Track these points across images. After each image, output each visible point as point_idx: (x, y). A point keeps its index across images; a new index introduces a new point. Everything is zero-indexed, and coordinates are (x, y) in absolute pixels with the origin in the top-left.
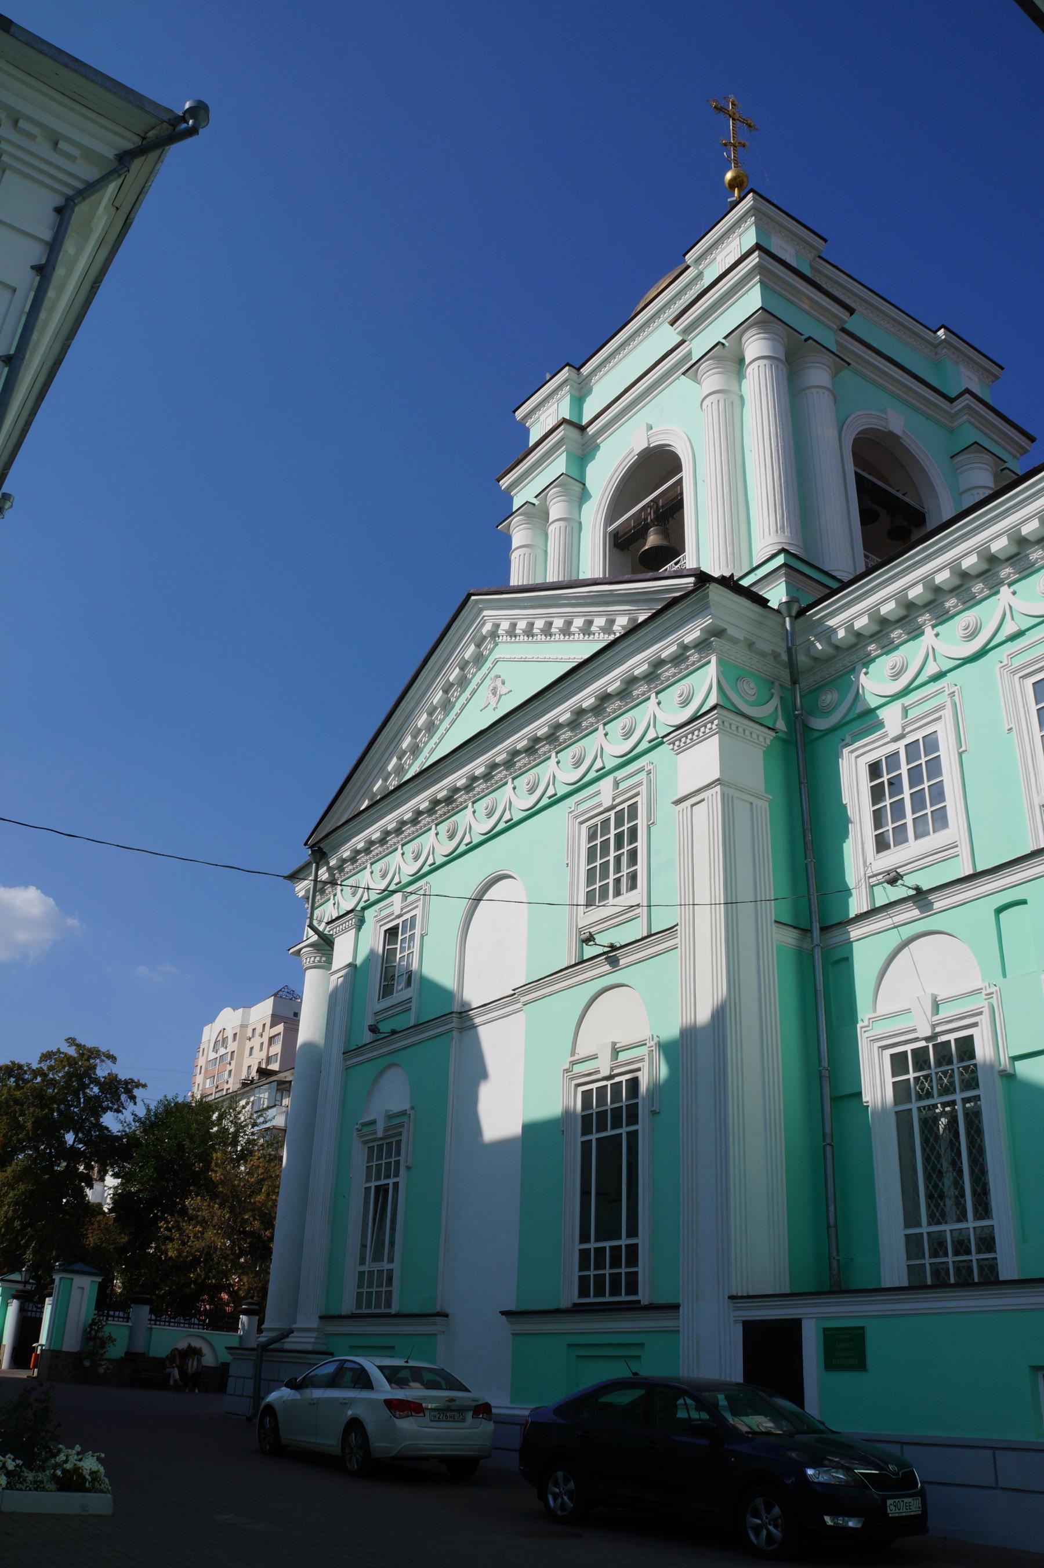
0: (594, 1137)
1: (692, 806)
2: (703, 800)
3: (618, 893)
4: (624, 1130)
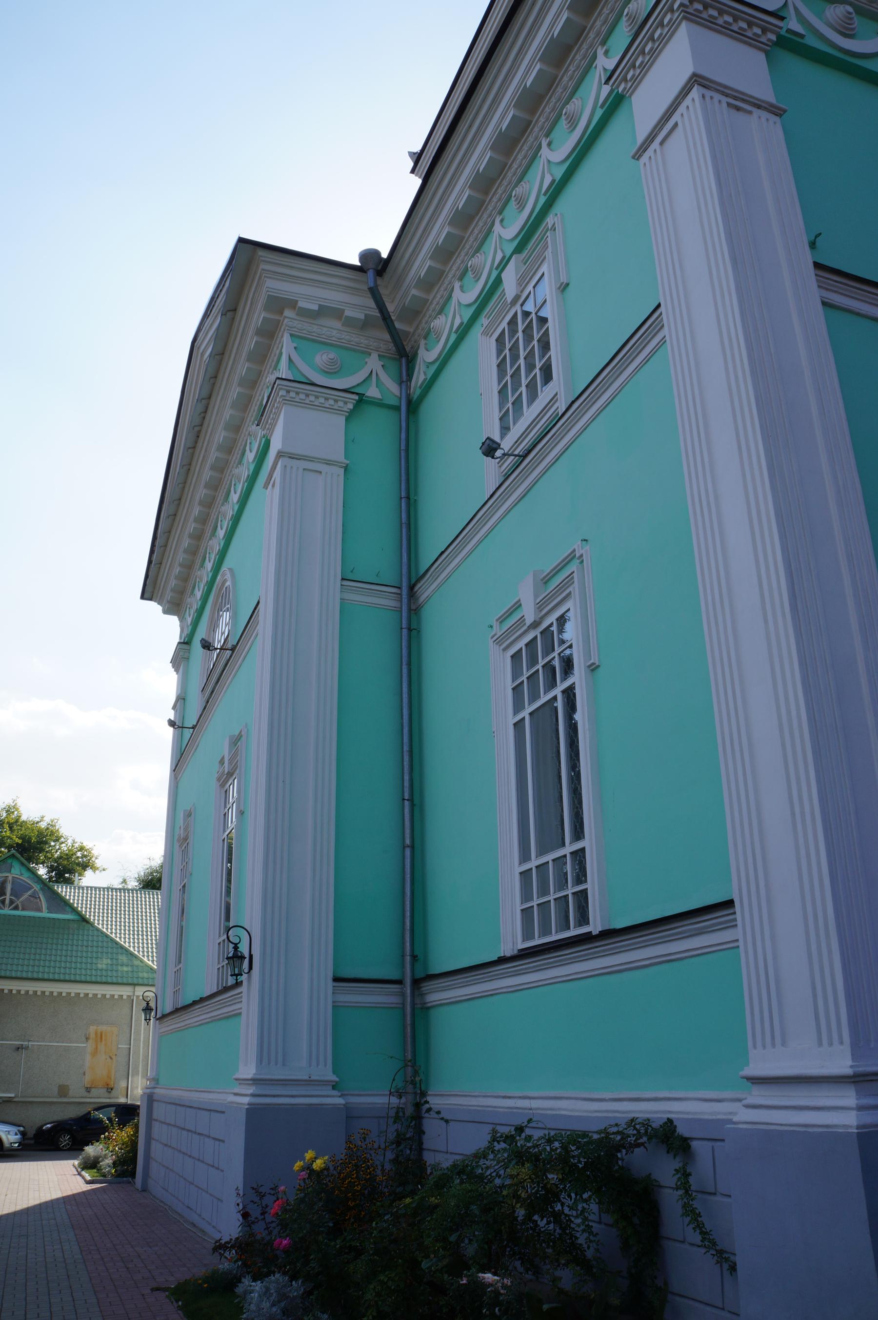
0: (525, 713)
1: (661, 143)
2: (676, 124)
4: (557, 691)
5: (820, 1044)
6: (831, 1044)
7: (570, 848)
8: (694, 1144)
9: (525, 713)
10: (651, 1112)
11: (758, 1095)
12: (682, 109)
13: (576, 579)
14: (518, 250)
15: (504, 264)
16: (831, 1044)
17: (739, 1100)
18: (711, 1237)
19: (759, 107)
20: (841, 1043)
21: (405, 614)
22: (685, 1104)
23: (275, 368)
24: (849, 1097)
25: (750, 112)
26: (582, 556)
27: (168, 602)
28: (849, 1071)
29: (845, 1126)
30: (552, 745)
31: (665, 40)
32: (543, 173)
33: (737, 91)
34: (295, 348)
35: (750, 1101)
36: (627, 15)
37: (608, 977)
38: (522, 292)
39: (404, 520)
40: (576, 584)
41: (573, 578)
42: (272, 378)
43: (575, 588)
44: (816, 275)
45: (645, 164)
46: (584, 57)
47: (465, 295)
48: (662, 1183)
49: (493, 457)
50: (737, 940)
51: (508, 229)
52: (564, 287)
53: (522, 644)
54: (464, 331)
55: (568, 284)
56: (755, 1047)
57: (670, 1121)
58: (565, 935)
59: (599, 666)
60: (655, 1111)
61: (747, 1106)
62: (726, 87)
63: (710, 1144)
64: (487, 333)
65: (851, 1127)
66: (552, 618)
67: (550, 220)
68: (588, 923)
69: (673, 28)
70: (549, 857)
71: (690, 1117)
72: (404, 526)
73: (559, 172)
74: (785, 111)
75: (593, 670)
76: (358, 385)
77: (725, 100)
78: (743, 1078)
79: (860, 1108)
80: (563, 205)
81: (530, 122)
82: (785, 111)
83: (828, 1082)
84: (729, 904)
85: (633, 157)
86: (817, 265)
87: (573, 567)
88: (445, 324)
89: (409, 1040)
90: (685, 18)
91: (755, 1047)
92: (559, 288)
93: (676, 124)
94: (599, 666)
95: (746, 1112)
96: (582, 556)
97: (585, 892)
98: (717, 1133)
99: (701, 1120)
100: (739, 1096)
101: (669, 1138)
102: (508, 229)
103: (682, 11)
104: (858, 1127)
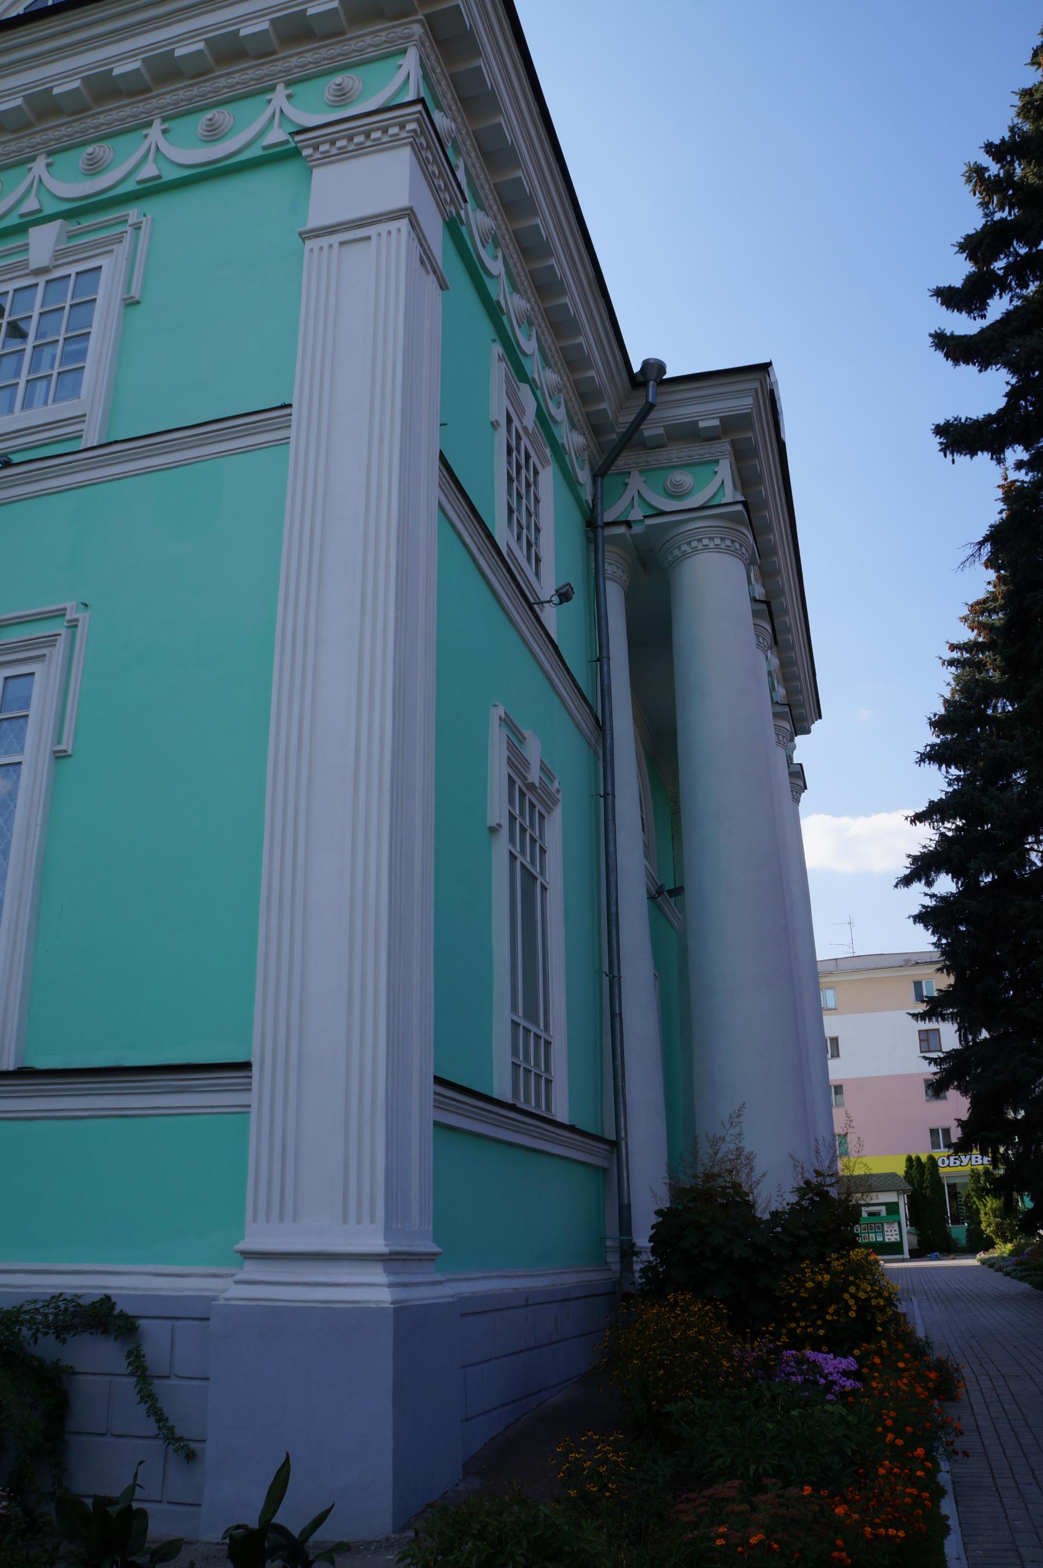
2: (369, 238)
3: (27, 404)
5: (345, 1221)
6: (359, 1222)
8: (142, 1323)
10: (81, 1287)
11: (253, 1270)
12: (383, 228)
14: (67, 215)
16: (281, 1219)
17: (232, 1275)
18: (169, 1424)
19: (435, 272)
20: (372, 1221)
22: (127, 1278)
24: (378, 1275)
25: (428, 272)
27: (943, 835)
28: (385, 1250)
29: (377, 1302)
31: (379, 147)
33: (429, 247)
35: (240, 1276)
37: (12, 1124)
38: (55, 267)
41: (56, 640)
43: (58, 652)
45: (312, 250)
46: (259, 79)
48: (77, 1370)
50: (249, 1106)
52: (131, 303)
55: (138, 302)
56: (255, 1220)
57: (108, 1298)
59: (70, 756)
60: (88, 1285)
61: (237, 1282)
62: (424, 237)
63: (170, 1323)
65: (384, 1302)
67: (133, 212)
69: (394, 144)
71: (141, 1293)
73: (171, 174)
74: (448, 289)
75: (58, 758)
78: (236, 1252)
79: (391, 1285)
81: (148, 90)
82: (448, 289)
83: (361, 1260)
84: (246, 1066)
85: (300, 234)
87: (57, 627)
90: (411, 144)
91: (255, 1220)
92: (125, 300)
94: (70, 756)
95: (235, 1289)
98: (197, 1313)
99: (155, 1296)
100: (231, 1272)
101: (103, 1318)
103: (412, 137)
104: (393, 1303)
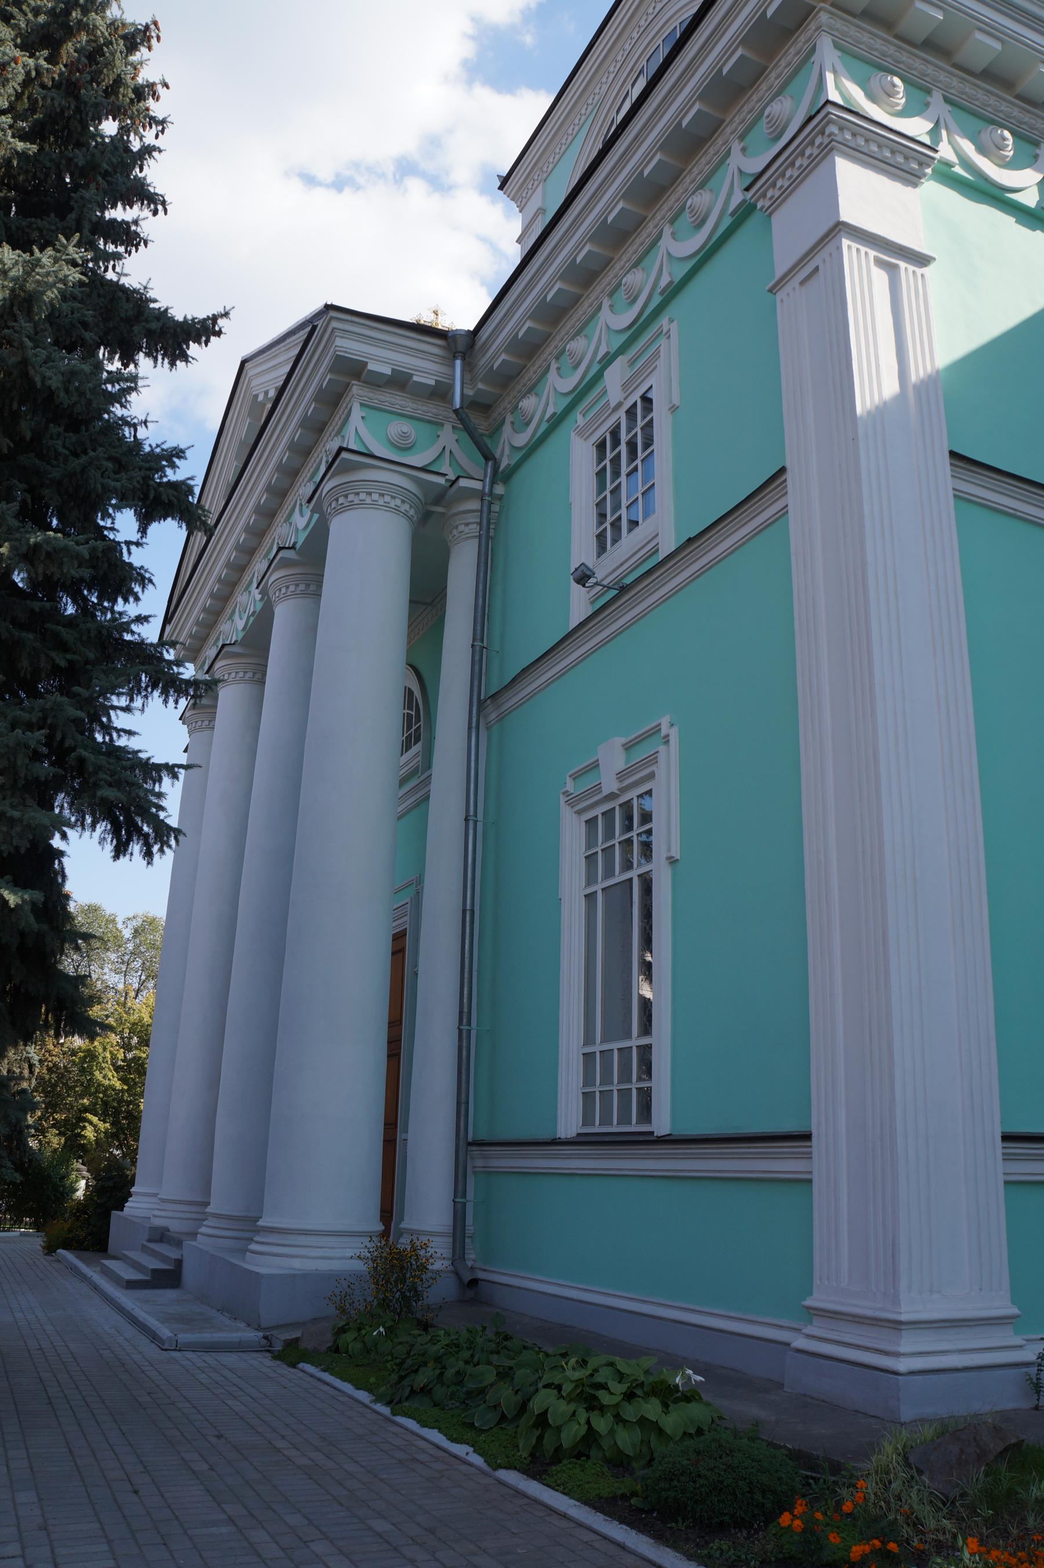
0: (598, 887)
2: (817, 269)
4: (634, 874)
7: (636, 1041)
9: (598, 887)
13: (662, 353)
15: (608, 360)
21: (483, 540)
23: (339, 432)
26: (668, 736)
30: (627, 916)
32: (662, 265)
34: (363, 418)
36: (768, 116)
39: (468, 907)
40: (662, 358)
42: (333, 445)
44: (951, 464)
47: (560, 382)
49: (584, 586)
51: (615, 318)
53: (598, 811)
54: (557, 421)
58: (623, 1136)
64: (583, 433)
66: (636, 397)
68: (650, 1122)
70: (615, 1046)
72: (468, 913)
76: (434, 461)
77: (872, 253)
80: (676, 308)
86: (953, 454)
88: (538, 406)
89: (480, 594)
93: (817, 269)
96: (668, 736)
97: (648, 1048)
102: (615, 318)
